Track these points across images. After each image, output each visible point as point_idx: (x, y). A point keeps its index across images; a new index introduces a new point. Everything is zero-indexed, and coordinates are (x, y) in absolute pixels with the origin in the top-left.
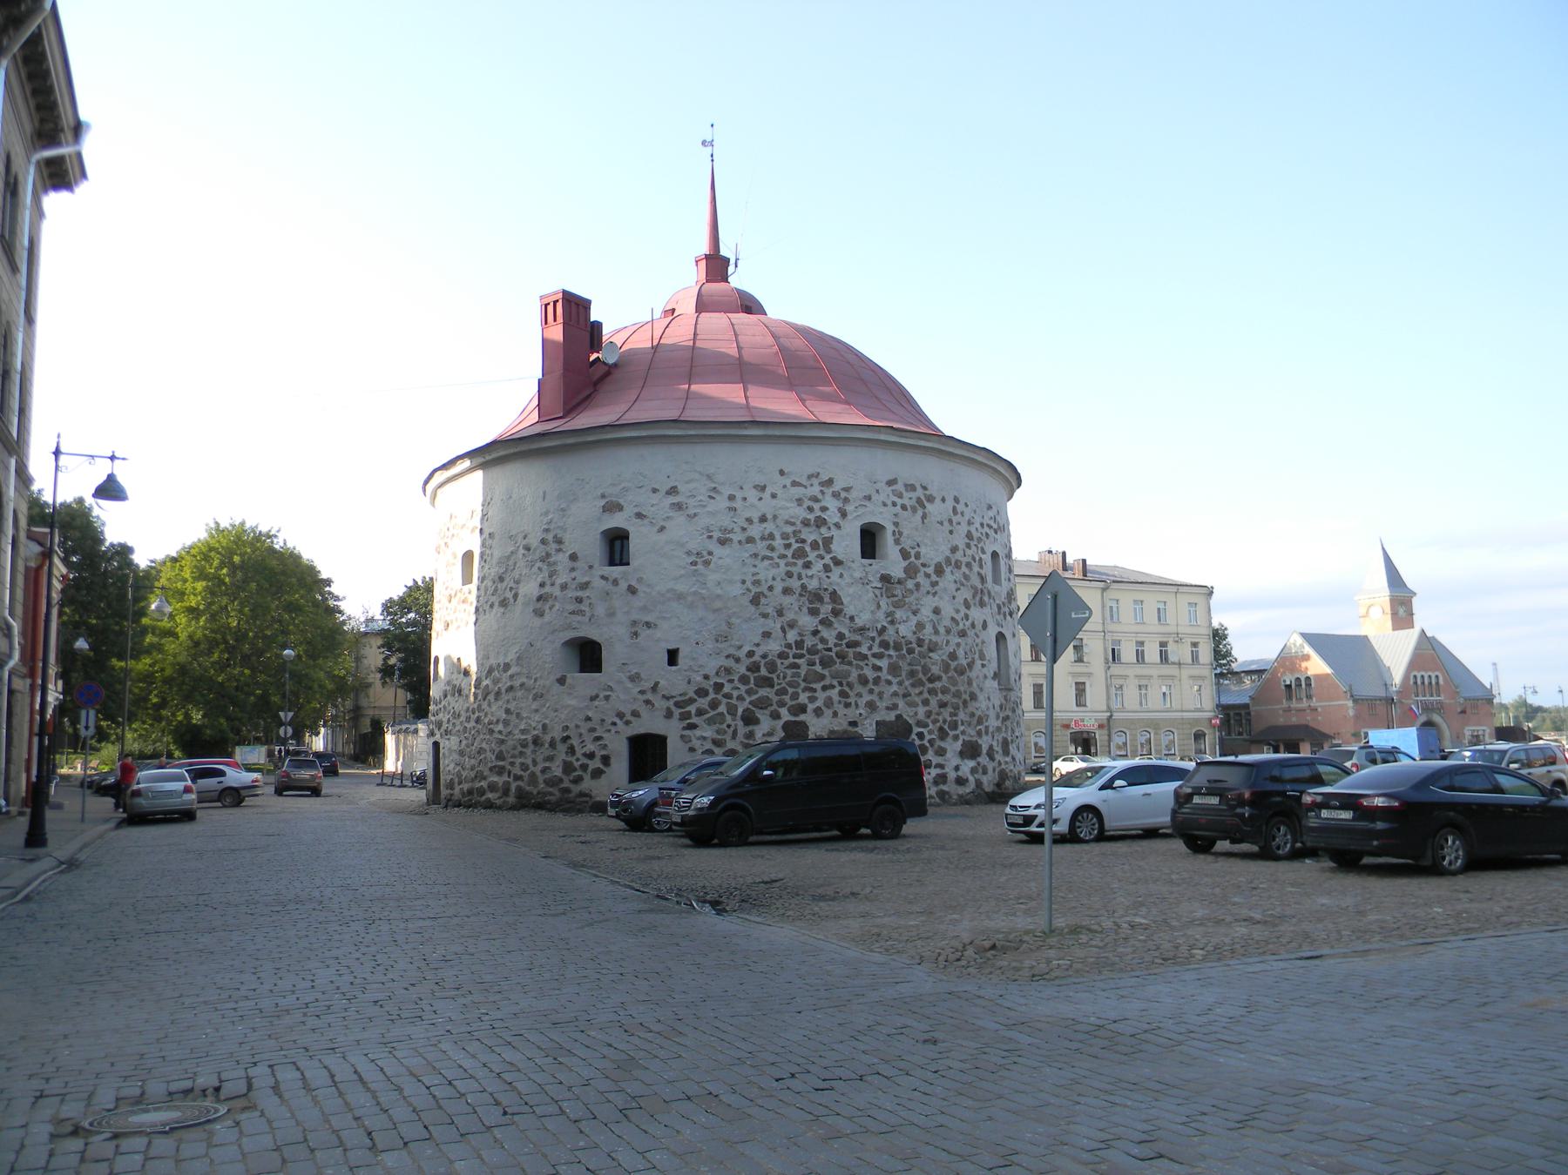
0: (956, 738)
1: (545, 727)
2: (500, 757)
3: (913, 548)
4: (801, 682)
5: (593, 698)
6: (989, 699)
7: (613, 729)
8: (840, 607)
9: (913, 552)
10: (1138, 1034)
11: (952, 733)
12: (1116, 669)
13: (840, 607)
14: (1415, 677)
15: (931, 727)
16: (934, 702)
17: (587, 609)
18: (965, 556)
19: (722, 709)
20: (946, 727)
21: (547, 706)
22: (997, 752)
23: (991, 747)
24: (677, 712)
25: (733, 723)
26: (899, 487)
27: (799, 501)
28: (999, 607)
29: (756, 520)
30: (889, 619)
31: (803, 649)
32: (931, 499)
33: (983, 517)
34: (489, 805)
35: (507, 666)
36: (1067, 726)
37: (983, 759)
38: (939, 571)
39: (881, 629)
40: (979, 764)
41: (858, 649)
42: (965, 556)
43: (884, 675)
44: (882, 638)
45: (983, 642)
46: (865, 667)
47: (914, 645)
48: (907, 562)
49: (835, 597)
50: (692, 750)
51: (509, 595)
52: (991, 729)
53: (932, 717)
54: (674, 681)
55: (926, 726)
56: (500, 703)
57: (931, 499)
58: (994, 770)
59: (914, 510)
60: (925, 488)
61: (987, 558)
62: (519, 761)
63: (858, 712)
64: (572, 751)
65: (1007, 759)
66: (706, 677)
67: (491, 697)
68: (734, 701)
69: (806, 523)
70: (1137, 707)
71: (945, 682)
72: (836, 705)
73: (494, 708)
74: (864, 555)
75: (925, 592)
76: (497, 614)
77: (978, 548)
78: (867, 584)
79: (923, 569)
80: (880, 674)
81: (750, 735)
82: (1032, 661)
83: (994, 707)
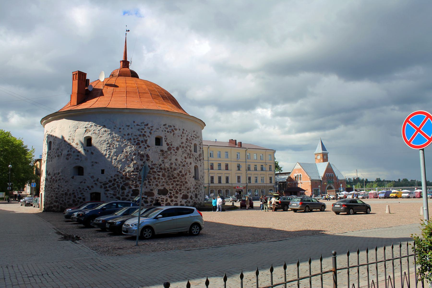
0: (181, 194)
1: (68, 190)
2: (56, 198)
3: (170, 143)
4: (137, 179)
5: (81, 182)
6: (191, 183)
7: (86, 191)
8: (149, 158)
9: (170, 144)
10: (230, 272)
11: (180, 192)
12: (248, 172)
13: (149, 158)
14: (327, 174)
15: (174, 191)
16: (175, 184)
17: (80, 158)
18: (185, 145)
19: (116, 186)
20: (178, 191)
21: (69, 184)
22: (193, 197)
23: (191, 196)
24: (103, 186)
25: (118, 190)
26: (167, 126)
27: (139, 130)
28: (196, 158)
29: (126, 135)
30: (163, 162)
31: (138, 170)
32: (176, 129)
33: (192, 134)
34: (54, 211)
35: (59, 173)
36: (235, 188)
37: (189, 199)
38: (177, 149)
39: (160, 165)
40: (187, 200)
41: (154, 170)
42: (185, 145)
43: (161, 177)
44: (160, 167)
45: (190, 168)
46: (155, 175)
47: (170, 169)
48: (168, 147)
49: (148, 156)
50: (107, 197)
51: (60, 154)
52: (192, 191)
53: (174, 188)
54: (103, 178)
55: (172, 190)
56: (57, 183)
57: (176, 129)
58: (192, 202)
59: (171, 132)
60: (174, 127)
61: (192, 146)
62: (61, 199)
63: (153, 187)
64: (75, 197)
65: (197, 199)
66: (112, 177)
67: (55, 182)
68: (119, 184)
69: (140, 135)
70: (261, 183)
71: (178, 179)
72: (147, 185)
73: (55, 185)
74: (156, 145)
75: (173, 154)
76: (56, 159)
77: (189, 142)
78: (157, 152)
79: (173, 148)
80: (159, 176)
81: (123, 193)
82: (226, 170)
83: (193, 185)
